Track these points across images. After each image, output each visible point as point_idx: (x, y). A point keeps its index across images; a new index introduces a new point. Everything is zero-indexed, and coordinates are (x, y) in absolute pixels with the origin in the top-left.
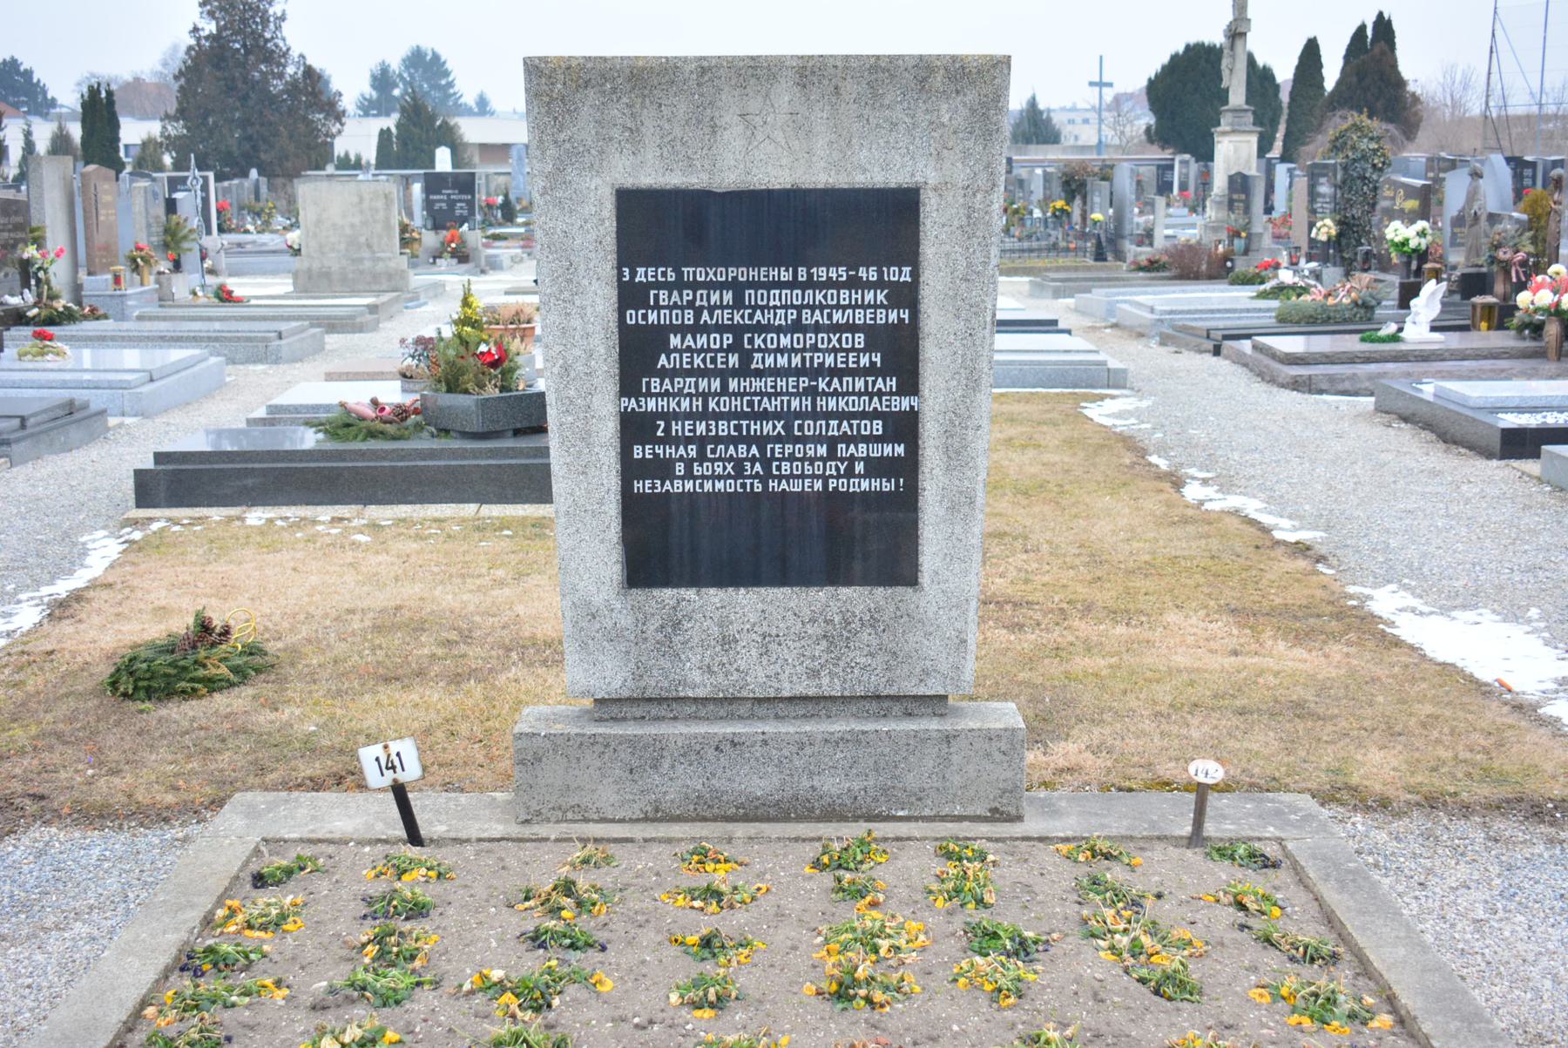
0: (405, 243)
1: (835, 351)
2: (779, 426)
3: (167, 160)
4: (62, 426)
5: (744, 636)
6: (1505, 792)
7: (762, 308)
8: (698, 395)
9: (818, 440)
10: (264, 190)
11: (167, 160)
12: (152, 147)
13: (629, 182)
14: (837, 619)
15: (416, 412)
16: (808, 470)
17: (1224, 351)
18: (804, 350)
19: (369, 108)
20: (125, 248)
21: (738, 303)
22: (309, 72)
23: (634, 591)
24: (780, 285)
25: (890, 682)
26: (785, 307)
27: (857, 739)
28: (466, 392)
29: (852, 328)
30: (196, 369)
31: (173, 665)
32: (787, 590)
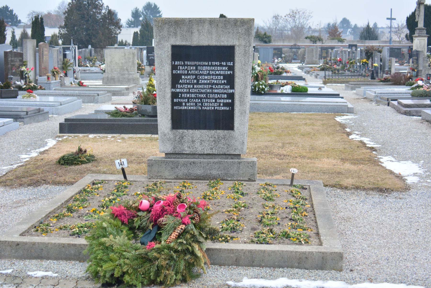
0: (139, 69)
1: (217, 80)
2: (205, 95)
3: (60, 42)
4: (37, 115)
5: (197, 140)
6: (376, 186)
7: (201, 70)
8: (188, 88)
9: (213, 98)
10: (93, 52)
11: (60, 42)
12: (55, 38)
13: (174, 44)
14: (217, 137)
15: (136, 110)
16: (211, 105)
17: (390, 104)
18: (210, 79)
19: (131, 24)
20: (51, 68)
21: (196, 69)
22: (110, 12)
23: (174, 130)
24: (205, 66)
25: (228, 151)
26: (206, 70)
27: (220, 163)
28: (150, 104)
29: (220, 75)
30: (74, 102)
31: (73, 157)
32: (206, 131)
